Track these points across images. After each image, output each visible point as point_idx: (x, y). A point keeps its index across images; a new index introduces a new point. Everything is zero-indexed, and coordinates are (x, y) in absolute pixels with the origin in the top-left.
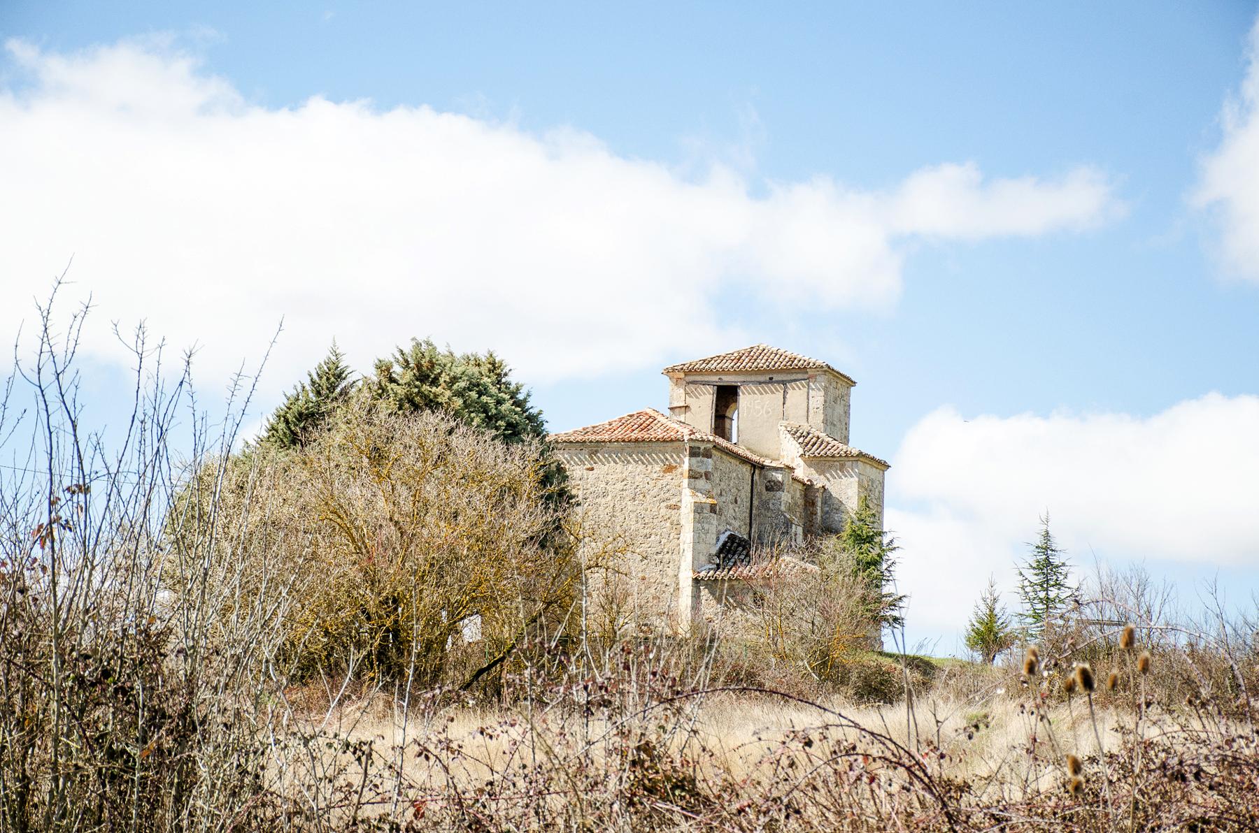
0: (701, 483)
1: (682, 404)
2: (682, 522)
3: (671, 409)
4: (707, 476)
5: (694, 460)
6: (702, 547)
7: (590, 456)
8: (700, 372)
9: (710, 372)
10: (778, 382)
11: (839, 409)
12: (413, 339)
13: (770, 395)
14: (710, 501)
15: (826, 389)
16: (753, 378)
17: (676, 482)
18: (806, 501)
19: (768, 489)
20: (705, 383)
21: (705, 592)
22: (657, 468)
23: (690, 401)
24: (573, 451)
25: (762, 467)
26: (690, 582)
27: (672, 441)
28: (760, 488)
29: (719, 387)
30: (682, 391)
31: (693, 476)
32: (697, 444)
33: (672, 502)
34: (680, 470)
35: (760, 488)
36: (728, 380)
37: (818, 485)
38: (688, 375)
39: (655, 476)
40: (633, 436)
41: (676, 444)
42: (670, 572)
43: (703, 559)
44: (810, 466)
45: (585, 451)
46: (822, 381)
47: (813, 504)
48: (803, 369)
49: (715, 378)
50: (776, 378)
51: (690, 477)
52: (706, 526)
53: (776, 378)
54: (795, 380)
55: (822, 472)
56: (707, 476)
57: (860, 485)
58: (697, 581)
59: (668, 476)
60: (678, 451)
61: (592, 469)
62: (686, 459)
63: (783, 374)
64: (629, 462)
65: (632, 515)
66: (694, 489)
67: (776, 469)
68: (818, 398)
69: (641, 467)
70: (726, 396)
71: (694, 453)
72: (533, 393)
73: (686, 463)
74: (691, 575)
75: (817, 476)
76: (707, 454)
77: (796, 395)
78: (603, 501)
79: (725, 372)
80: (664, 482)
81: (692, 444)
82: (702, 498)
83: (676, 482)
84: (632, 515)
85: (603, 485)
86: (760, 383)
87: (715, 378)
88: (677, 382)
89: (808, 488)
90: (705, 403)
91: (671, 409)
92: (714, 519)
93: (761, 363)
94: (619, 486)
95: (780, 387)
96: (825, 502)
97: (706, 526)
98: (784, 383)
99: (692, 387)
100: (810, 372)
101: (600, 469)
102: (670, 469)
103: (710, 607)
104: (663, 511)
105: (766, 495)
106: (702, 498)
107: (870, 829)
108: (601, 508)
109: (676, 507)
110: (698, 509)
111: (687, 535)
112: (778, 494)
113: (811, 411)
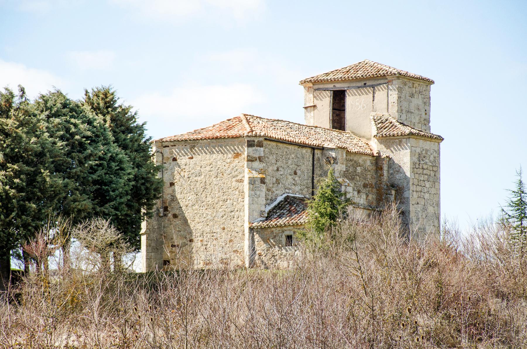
0: (256, 164)
1: (312, 104)
2: (245, 191)
3: (306, 108)
4: (260, 159)
5: (251, 149)
6: (255, 206)
7: (191, 149)
8: (321, 82)
9: (327, 81)
10: (369, 86)
11: (417, 101)
12: (19, 86)
13: (366, 96)
14: (260, 176)
15: (400, 90)
16: (354, 85)
17: (241, 164)
18: (377, 167)
20: (325, 90)
21: (257, 237)
22: (230, 156)
23: (317, 102)
24: (180, 147)
25: (323, 149)
26: (248, 228)
27: (237, 137)
29: (334, 91)
30: (312, 95)
31: (250, 160)
32: (252, 139)
33: (239, 178)
34: (243, 156)
36: (339, 86)
37: (384, 156)
38: (315, 85)
39: (229, 161)
40: (218, 134)
41: (240, 139)
42: (239, 224)
43: (256, 214)
44: (381, 143)
45: (188, 146)
46: (397, 83)
47: (381, 169)
48: (384, 76)
49: (331, 86)
50: (368, 83)
51: (248, 161)
52: (258, 193)
53: (368, 83)
54: (380, 84)
55: (388, 147)
56: (260, 159)
57: (412, 154)
58: (251, 229)
59: (237, 160)
60: (241, 144)
61: (192, 158)
62: (246, 149)
63: (373, 80)
64: (213, 153)
66: (251, 168)
67: (331, 149)
68: (394, 96)
69: (221, 155)
70: (339, 99)
71: (250, 144)
72: (139, 113)
73: (246, 151)
75: (385, 149)
76: (260, 145)
77: (381, 94)
79: (335, 81)
80: (234, 164)
81: (249, 139)
82: (255, 175)
83: (241, 164)
84: (216, 187)
85: (199, 168)
86: (359, 87)
87: (331, 86)
88: (308, 89)
89: (377, 160)
90: (325, 103)
91: (306, 108)
92: (264, 188)
93: (359, 74)
94: (208, 168)
95: (371, 90)
96: (390, 167)
97: (258, 193)
98: (373, 87)
99: (318, 92)
100: (389, 78)
101: (197, 158)
102: (237, 155)
103: (261, 247)
104: (234, 184)
106: (255, 175)
108: (198, 184)
109: (241, 181)
110: (252, 181)
113: (390, 105)
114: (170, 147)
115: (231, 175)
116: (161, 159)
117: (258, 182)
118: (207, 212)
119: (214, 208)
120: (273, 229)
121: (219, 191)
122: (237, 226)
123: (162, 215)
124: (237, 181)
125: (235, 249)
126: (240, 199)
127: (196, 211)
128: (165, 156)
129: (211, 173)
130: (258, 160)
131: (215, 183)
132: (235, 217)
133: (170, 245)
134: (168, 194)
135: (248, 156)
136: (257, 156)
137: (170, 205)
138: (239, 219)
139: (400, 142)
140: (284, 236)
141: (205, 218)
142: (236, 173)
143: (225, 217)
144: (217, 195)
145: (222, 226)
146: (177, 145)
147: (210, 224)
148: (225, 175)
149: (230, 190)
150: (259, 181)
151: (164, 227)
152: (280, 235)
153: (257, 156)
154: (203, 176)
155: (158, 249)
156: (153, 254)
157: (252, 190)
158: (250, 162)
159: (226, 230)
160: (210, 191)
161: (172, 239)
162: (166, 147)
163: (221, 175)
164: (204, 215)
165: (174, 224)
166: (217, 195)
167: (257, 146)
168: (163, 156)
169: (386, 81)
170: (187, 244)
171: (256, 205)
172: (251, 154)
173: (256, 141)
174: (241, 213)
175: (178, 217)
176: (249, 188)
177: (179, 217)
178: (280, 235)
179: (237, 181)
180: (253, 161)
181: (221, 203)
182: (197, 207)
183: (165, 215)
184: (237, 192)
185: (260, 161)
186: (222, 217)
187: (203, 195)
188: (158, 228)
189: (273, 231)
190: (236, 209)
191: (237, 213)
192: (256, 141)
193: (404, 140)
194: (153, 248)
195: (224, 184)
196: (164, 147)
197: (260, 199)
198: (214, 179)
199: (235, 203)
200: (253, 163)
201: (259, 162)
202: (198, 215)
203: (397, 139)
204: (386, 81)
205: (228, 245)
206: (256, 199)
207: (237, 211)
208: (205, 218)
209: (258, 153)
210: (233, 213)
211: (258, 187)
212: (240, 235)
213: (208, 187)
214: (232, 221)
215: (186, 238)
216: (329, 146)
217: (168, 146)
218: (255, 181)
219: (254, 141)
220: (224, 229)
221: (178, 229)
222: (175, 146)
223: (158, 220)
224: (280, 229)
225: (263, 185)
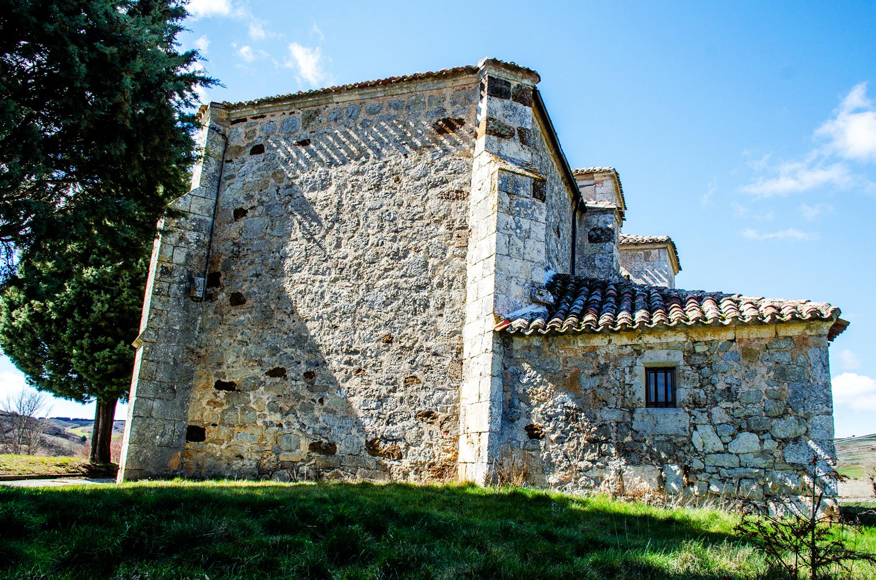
5: (497, 103)
6: (515, 266)
19: (591, 240)
26: (488, 341)
28: (582, 238)
32: (504, 75)
35: (582, 238)
41: (462, 81)
42: (443, 326)
43: (517, 291)
51: (489, 132)
52: (526, 224)
58: (504, 338)
65: (372, 217)
74: (491, 324)
78: (321, 195)
81: (494, 73)
84: (372, 217)
97: (526, 224)
104: (433, 204)
105: (589, 248)
107: (14, 180)
109: (460, 195)
110: (508, 186)
111: (484, 243)
112: (608, 246)
114: (249, 120)
115: (424, 181)
116: (219, 150)
117: (525, 191)
118: (335, 289)
119: (360, 277)
120: (597, 341)
121: (381, 228)
122: (438, 333)
123: (199, 294)
124: (447, 196)
125: (423, 408)
126: (451, 249)
127: (302, 287)
128: (233, 143)
129: (360, 178)
130: (517, 137)
131: (368, 204)
132: (432, 303)
133: (214, 380)
134: (226, 240)
135: (489, 119)
136: (515, 125)
137: (227, 268)
138: (447, 310)
139: (647, 255)
140: (640, 370)
141: (326, 305)
142: (442, 174)
143: (395, 304)
144: (372, 239)
145: (383, 332)
146: (268, 115)
147: (342, 326)
148: (404, 180)
149: (419, 223)
150: (529, 187)
151: (202, 330)
152: (626, 363)
153: (515, 127)
154: (332, 189)
155: (174, 391)
156: (156, 404)
157: (509, 212)
158: (495, 138)
159: (395, 346)
160: (350, 226)
161: (220, 365)
162: (238, 121)
163: (392, 182)
164: (327, 299)
165: (233, 320)
166: (372, 239)
167: (516, 99)
168: (227, 144)
169: (592, 182)
170: (262, 383)
171: (519, 263)
172: (498, 116)
173: (514, 84)
174: (454, 294)
175: (244, 302)
176: (500, 203)
177: (250, 302)
178: (626, 363)
179: (447, 196)
180: (503, 136)
181: (384, 262)
182: (304, 274)
183: (209, 297)
184: (442, 229)
185: (523, 141)
186: (385, 304)
187: (329, 239)
188: (186, 331)
189: (594, 349)
190: (436, 281)
191: (438, 293)
192: (514, 84)
193: (655, 252)
194: (160, 386)
195: (400, 205)
196: (233, 123)
197: (530, 243)
198: (368, 195)
199: (432, 262)
200: (504, 143)
201: (519, 144)
202: (308, 298)
203: (641, 249)
204: (592, 182)
205: (398, 395)
206: (520, 244)
207: (440, 285)
208: (326, 305)
209: (517, 118)
210: (424, 293)
211: (526, 207)
212: (447, 363)
213: (345, 216)
214: (420, 318)
215: (260, 363)
216: (601, 205)
217: (245, 120)
218: (516, 185)
219: (508, 84)
220: (389, 341)
221: (240, 337)
222: (263, 117)
223: (186, 308)
224: (625, 340)
225: (539, 202)
